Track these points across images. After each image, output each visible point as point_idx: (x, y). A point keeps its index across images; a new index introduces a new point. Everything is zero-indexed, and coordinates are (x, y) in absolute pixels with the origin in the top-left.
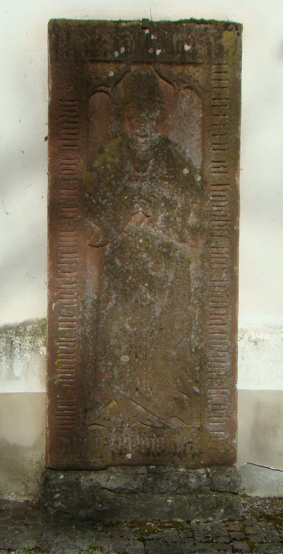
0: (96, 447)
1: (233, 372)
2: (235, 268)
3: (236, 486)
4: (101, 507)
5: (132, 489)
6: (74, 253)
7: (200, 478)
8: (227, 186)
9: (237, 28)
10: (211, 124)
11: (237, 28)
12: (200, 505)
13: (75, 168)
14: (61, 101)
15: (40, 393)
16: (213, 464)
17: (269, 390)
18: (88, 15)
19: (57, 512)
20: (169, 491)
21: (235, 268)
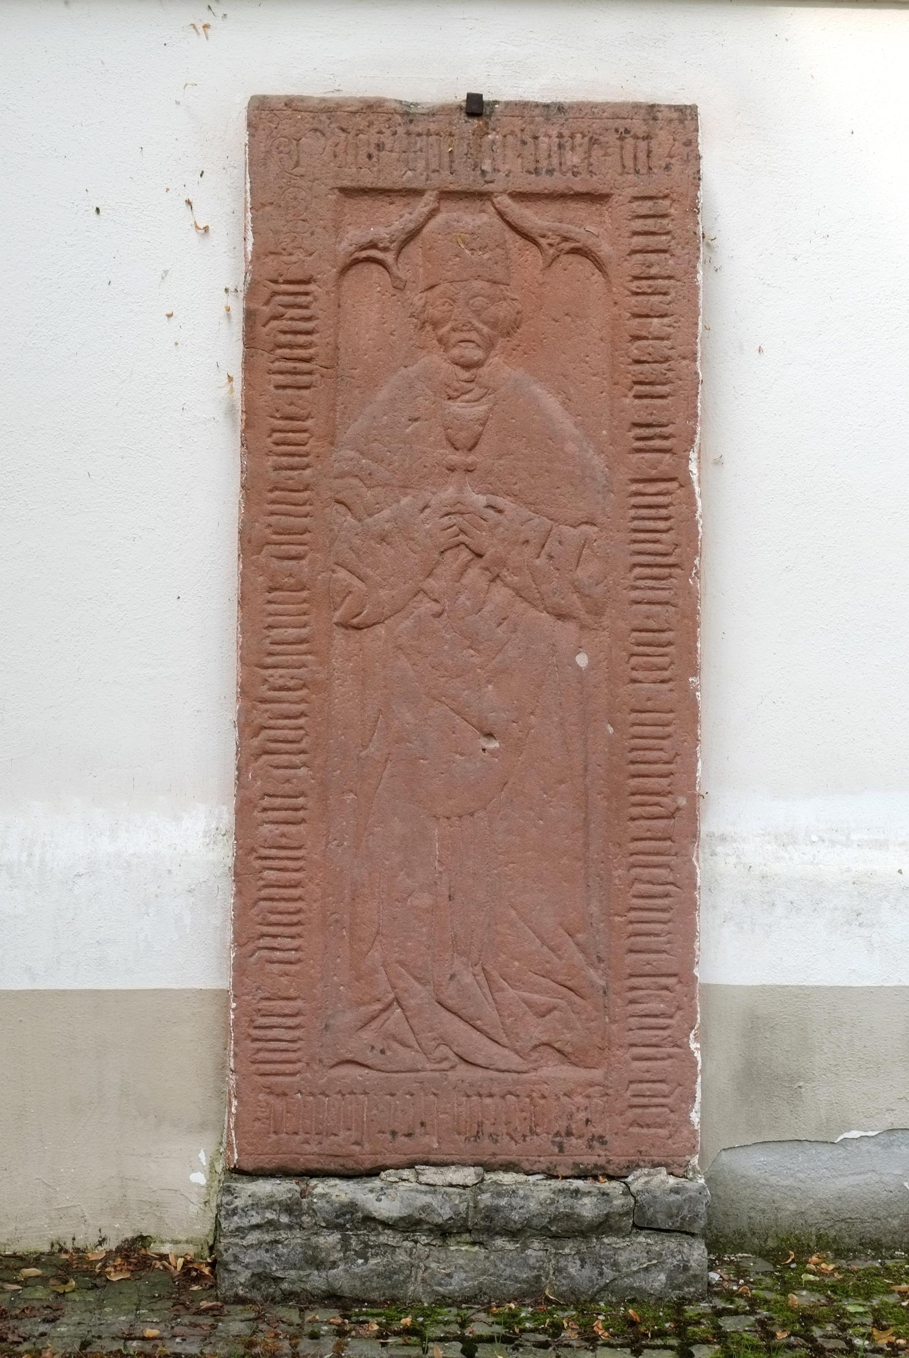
0: (352, 667)
1: (688, 958)
2: (690, 680)
3: (697, 1216)
4: (362, 1264)
5: (440, 1221)
6: (297, 797)
7: (608, 1194)
8: (664, 237)
9: (693, 109)
10: (631, 336)
11: (693, 109)
12: (607, 1263)
13: (306, 440)
14: (276, 282)
15: (215, 990)
16: (642, 1164)
17: (779, 986)
18: (340, 88)
19: (253, 1275)
20: (530, 1227)
21: (690, 680)
